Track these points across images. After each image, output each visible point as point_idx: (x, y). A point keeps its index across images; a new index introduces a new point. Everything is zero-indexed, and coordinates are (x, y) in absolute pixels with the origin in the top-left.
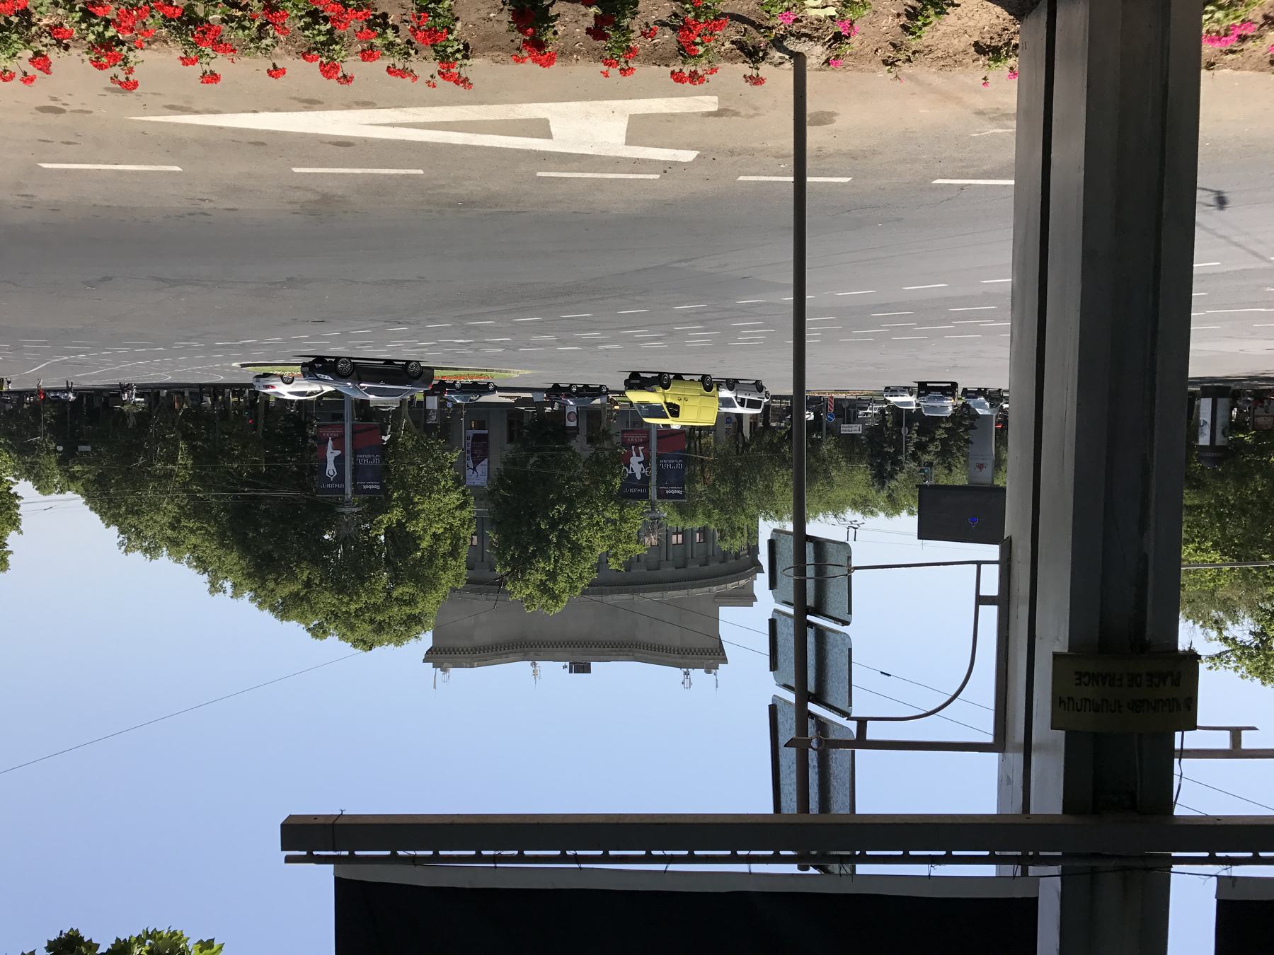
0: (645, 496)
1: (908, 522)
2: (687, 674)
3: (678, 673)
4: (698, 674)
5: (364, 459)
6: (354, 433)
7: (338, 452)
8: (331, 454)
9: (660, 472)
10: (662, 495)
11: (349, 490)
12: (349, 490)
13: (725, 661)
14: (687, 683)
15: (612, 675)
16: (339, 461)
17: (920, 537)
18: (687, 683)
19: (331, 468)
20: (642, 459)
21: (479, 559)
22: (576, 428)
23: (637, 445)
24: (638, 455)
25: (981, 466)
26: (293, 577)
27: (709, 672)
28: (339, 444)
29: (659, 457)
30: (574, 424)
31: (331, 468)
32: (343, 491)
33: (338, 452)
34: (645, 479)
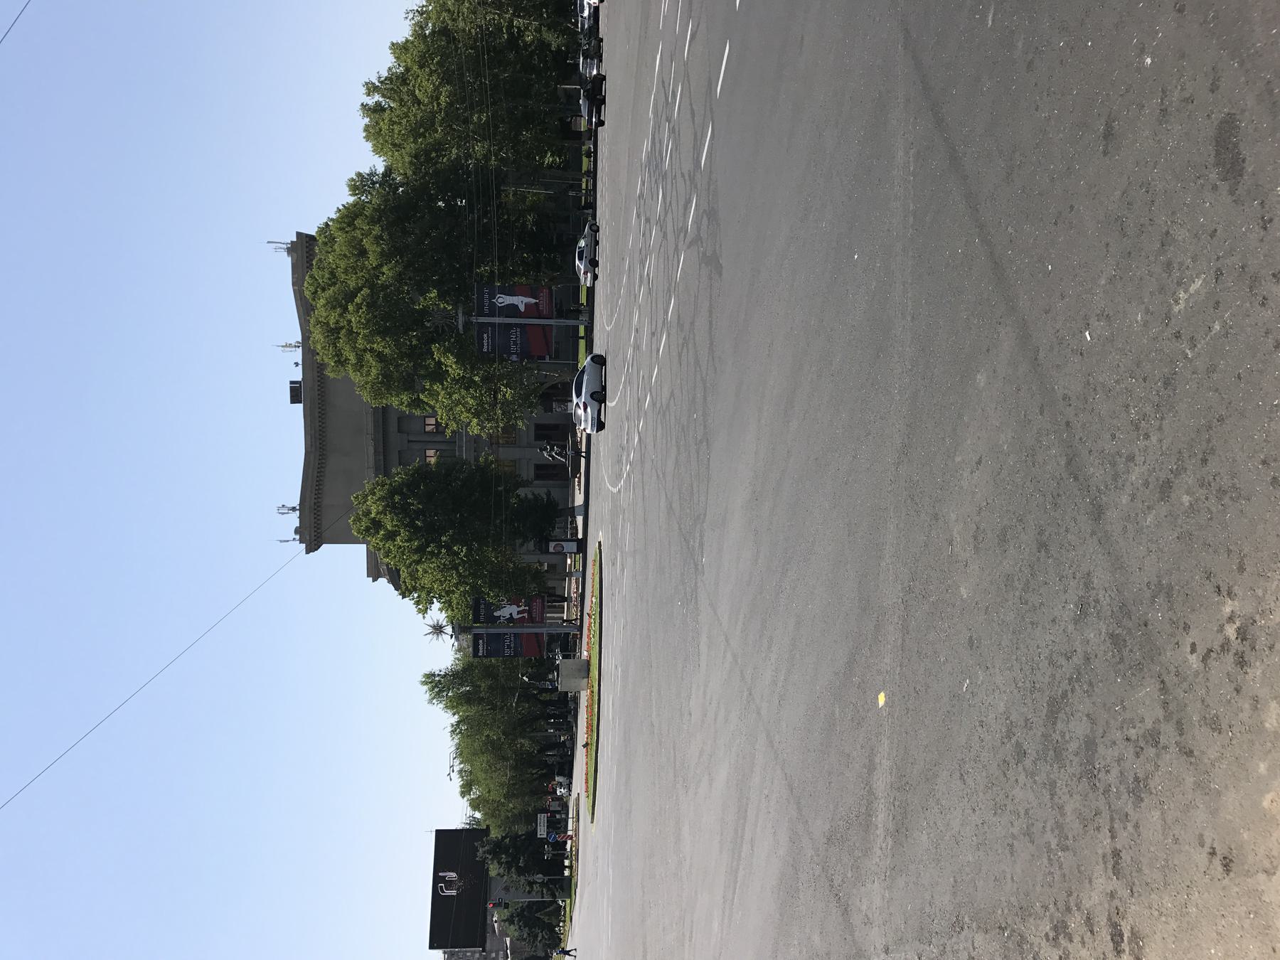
0: (476, 620)
1: (457, 813)
2: (294, 509)
3: (296, 502)
4: (294, 520)
5: (515, 335)
6: (543, 326)
7: (522, 308)
8: (521, 301)
9: (499, 637)
10: (476, 638)
11: (482, 320)
12: (482, 320)
13: (308, 551)
14: (284, 509)
15: (292, 423)
16: (512, 310)
17: (440, 834)
18: (284, 509)
19: (504, 300)
20: (515, 616)
21: (411, 438)
22: (547, 552)
23: (529, 612)
24: (519, 613)
25: (507, 889)
26: (386, 257)
27: (296, 531)
28: (532, 311)
29: (492, 325)
30: (551, 550)
31: (504, 300)
32: (481, 314)
33: (522, 308)
34: (493, 620)
